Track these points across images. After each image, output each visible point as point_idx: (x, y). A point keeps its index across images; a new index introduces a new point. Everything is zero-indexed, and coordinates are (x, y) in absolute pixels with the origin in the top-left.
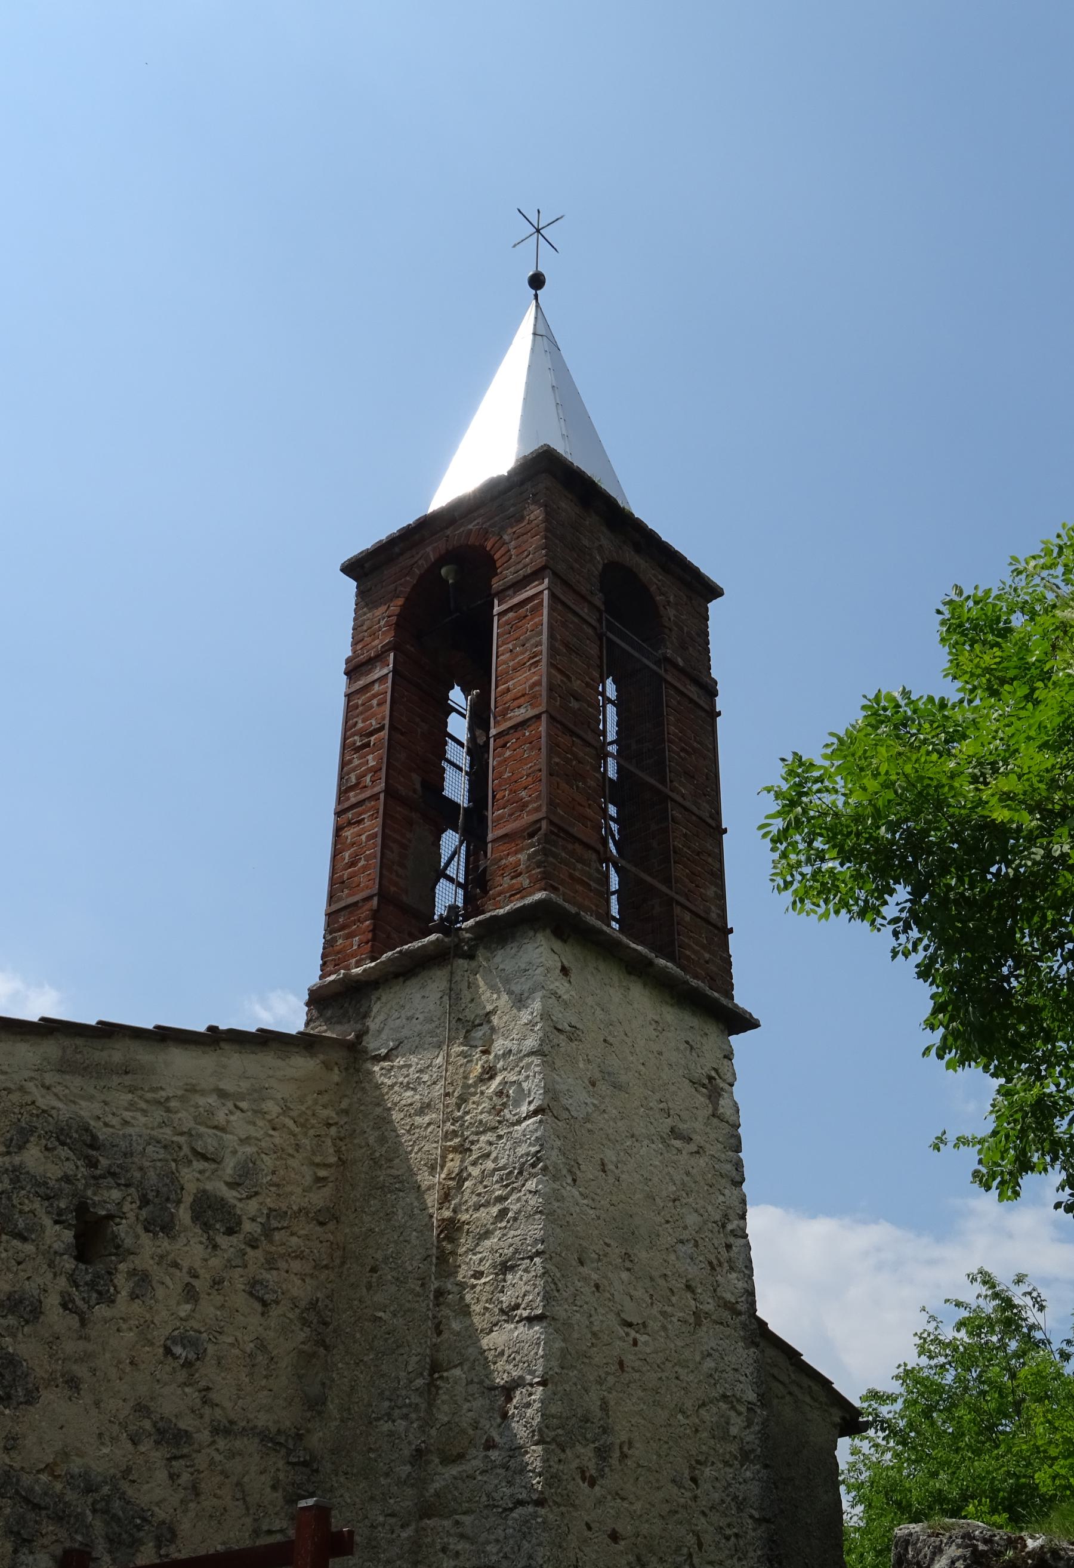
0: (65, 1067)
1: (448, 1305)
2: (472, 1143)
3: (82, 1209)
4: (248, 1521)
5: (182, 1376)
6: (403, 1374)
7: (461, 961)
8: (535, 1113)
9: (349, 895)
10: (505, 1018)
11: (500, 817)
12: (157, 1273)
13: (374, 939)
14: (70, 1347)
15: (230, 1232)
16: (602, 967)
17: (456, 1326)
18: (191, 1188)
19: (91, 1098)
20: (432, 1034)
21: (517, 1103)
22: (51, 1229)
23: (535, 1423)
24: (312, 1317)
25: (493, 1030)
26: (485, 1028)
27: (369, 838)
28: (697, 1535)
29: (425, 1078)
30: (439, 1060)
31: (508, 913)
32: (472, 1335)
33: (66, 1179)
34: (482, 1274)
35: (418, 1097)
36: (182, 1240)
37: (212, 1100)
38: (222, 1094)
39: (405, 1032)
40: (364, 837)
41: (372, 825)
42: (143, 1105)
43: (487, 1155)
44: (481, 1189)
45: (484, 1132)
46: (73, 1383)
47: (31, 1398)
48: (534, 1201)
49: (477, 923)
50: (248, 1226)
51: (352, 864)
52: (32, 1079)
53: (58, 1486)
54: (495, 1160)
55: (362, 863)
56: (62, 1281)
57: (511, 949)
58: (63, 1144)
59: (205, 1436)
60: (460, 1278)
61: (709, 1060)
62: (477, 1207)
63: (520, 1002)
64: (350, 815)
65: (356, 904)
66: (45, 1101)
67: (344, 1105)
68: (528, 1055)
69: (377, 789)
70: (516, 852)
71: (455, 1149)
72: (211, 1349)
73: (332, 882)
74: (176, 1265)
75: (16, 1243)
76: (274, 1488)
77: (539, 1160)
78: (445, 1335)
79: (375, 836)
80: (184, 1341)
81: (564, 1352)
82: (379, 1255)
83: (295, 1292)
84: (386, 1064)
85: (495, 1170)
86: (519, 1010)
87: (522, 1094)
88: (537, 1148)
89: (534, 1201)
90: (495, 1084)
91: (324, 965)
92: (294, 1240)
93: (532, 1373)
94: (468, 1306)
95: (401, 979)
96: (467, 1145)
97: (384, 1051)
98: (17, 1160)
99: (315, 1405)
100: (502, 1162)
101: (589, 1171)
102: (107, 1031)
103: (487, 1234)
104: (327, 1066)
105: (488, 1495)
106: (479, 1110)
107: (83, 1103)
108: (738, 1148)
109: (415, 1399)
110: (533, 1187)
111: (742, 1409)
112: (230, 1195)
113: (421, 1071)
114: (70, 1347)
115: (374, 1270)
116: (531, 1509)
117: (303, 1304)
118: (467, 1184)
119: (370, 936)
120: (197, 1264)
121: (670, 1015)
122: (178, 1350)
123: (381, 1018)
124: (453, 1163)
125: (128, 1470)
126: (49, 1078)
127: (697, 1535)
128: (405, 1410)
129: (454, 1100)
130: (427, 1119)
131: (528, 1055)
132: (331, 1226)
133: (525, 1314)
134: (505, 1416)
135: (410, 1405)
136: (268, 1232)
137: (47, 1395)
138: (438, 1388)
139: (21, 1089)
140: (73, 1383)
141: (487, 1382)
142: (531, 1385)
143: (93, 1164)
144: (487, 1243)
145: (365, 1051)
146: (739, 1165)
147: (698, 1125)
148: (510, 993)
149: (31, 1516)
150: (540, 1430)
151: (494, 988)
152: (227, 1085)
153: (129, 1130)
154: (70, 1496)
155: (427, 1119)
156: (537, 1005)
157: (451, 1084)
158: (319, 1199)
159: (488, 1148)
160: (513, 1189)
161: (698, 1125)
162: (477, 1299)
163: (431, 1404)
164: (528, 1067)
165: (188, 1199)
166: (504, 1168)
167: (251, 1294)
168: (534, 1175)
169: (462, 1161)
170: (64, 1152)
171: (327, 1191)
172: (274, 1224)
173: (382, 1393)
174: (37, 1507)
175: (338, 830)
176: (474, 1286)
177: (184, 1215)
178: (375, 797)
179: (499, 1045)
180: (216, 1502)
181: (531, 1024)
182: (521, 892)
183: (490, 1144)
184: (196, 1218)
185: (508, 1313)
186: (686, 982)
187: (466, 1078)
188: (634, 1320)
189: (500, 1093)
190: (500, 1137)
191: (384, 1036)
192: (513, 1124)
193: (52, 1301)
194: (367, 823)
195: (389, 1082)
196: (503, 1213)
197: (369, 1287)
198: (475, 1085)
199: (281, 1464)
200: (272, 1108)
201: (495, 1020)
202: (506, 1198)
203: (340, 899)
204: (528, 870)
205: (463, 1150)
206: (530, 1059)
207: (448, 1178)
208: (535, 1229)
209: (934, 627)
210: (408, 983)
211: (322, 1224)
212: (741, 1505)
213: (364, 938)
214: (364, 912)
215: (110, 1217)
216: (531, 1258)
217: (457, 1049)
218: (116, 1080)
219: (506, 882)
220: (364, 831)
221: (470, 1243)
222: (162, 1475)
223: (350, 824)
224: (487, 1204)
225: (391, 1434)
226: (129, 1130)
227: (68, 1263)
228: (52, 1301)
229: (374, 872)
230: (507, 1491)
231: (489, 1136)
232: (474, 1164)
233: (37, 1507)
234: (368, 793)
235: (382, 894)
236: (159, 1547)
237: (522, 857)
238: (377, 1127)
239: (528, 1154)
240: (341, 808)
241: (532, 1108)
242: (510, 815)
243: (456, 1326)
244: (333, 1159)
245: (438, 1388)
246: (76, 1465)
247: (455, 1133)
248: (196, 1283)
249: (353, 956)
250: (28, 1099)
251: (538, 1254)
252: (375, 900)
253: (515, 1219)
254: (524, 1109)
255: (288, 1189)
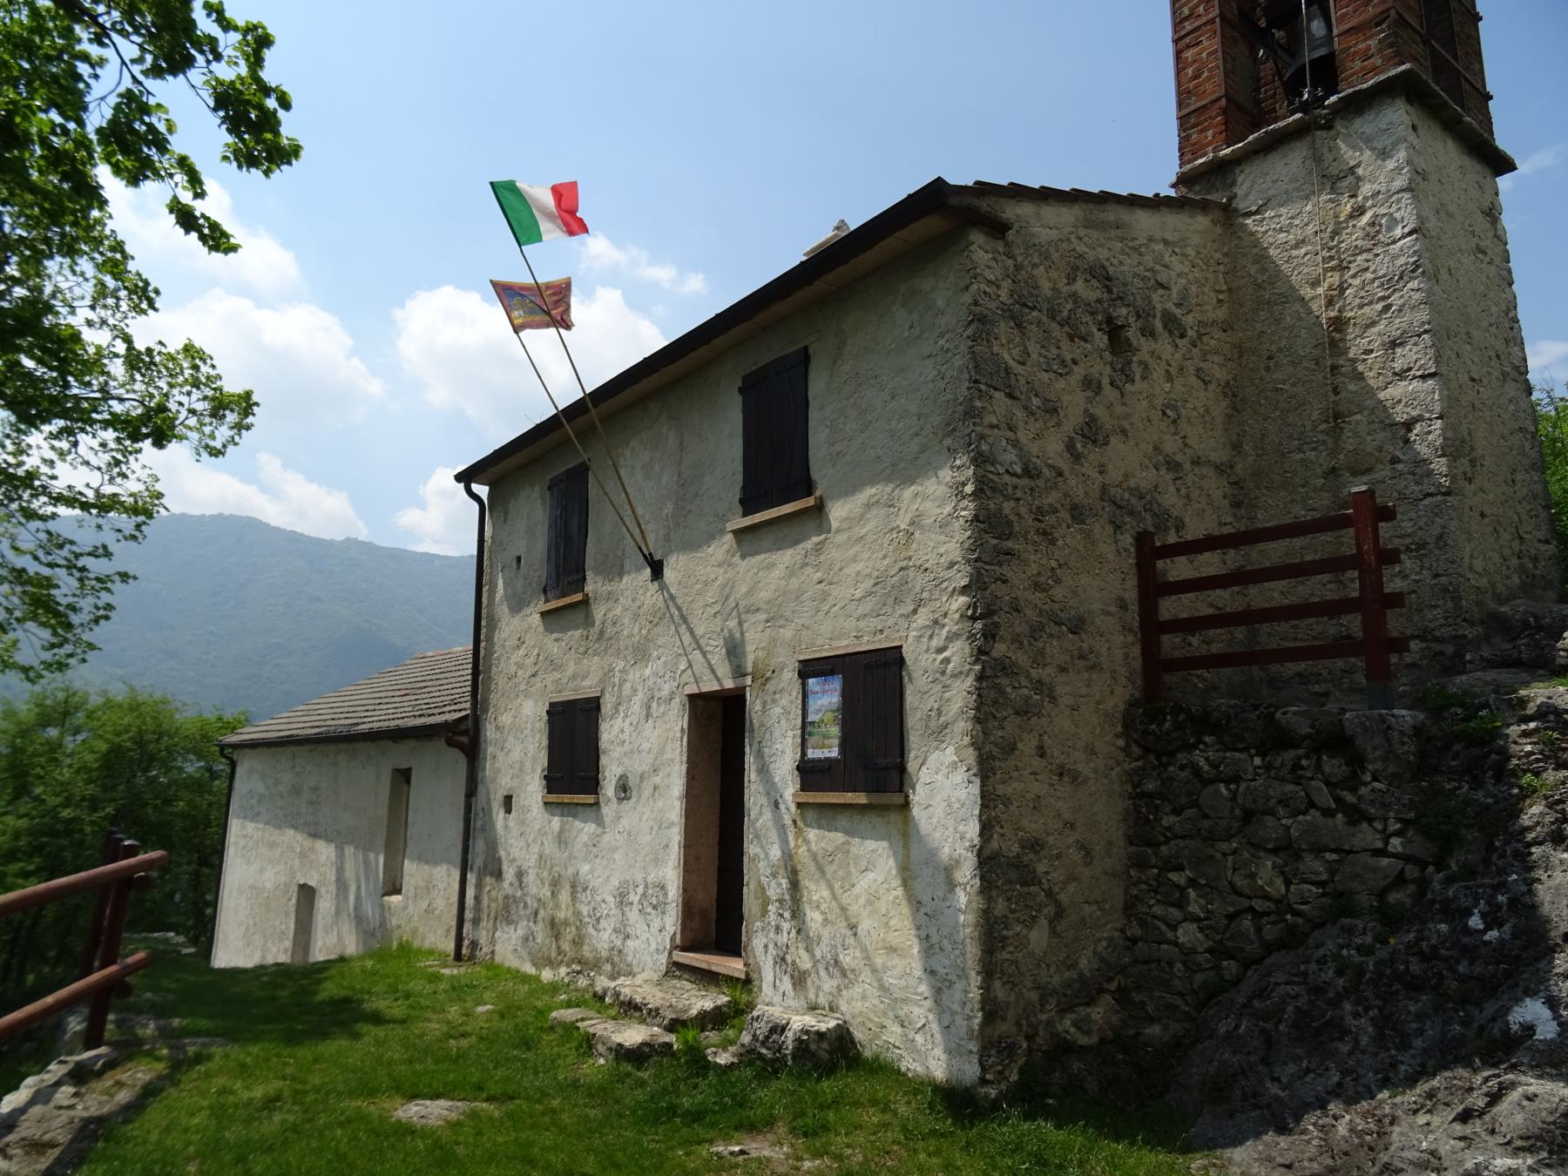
0: (1089, 224)
1: (1343, 375)
2: (1350, 262)
3: (1110, 320)
4: (1215, 516)
5: (1172, 428)
6: (1307, 423)
7: (1318, 133)
8: (1410, 234)
9: (1196, 101)
10: (1370, 169)
11: (1344, 15)
12: (1152, 362)
13: (1226, 130)
14: (1119, 410)
15: (1182, 336)
16: (1432, 125)
17: (1352, 387)
18: (1159, 306)
19: (1102, 246)
20: (1298, 190)
21: (1390, 229)
22: (1098, 334)
23: (1438, 443)
24: (1227, 391)
25: (1359, 179)
26: (1350, 179)
27: (1209, 54)
28: (1518, 515)
29: (1297, 222)
30: (1309, 208)
31: (1372, 86)
32: (1370, 392)
33: (1099, 301)
34: (1372, 351)
35: (1292, 237)
36: (1160, 342)
37: (1161, 246)
38: (1166, 242)
39: (1272, 192)
40: (1204, 55)
41: (1210, 44)
42: (1127, 250)
43: (1366, 269)
44: (1362, 293)
45: (1360, 253)
46: (1124, 432)
47: (1106, 443)
48: (1417, 296)
49: (1340, 99)
50: (1190, 332)
51: (1196, 77)
52: (1072, 233)
53: (1127, 495)
54: (1375, 271)
55: (1206, 74)
56: (1108, 368)
57: (1369, 116)
58: (1094, 277)
59: (1188, 466)
60: (1351, 355)
61: (1488, 198)
62: (1361, 306)
63: (1384, 154)
64: (1187, 40)
65: (1204, 106)
66: (1081, 248)
67: (1225, 250)
68: (1398, 192)
69: (1211, 16)
70: (1365, 40)
71: (1333, 269)
72: (1183, 411)
73: (1179, 93)
74: (1160, 358)
75: (1082, 343)
76: (1224, 497)
77: (1418, 267)
78: (1343, 395)
79: (1216, 51)
80: (1169, 406)
81: (1449, 397)
82: (1273, 347)
83: (1218, 376)
84: (1258, 217)
85: (1375, 279)
86: (1384, 160)
87: (1394, 222)
88: (1415, 258)
89: (1417, 296)
90: (1366, 219)
91: (1182, 156)
92: (1213, 342)
93: (1431, 412)
94: (1362, 373)
95: (1261, 155)
96: (1345, 264)
97: (1254, 208)
98: (1073, 288)
99: (1236, 447)
100: (1381, 273)
101: (1444, 275)
102: (1105, 198)
103: (1373, 324)
104: (1214, 222)
105: (1399, 493)
106: (1353, 237)
107: (1100, 250)
108: (1508, 262)
109: (1321, 437)
110: (1416, 286)
111: (1529, 436)
112: (1177, 312)
113: (1292, 218)
114: (1119, 410)
115: (1270, 358)
116: (1440, 498)
117: (1223, 383)
118: (1348, 292)
119: (1223, 127)
120: (1169, 357)
121: (1469, 163)
122: (1169, 412)
123: (1248, 184)
124: (1334, 278)
125: (1156, 487)
126: (1082, 232)
127: (1518, 515)
128: (1313, 445)
129: (1327, 234)
130: (1303, 251)
131: (1398, 192)
132: (1230, 332)
133: (1420, 373)
134: (1407, 441)
135: (1318, 441)
136: (1200, 335)
137: (1114, 440)
138: (1342, 429)
139: (1068, 240)
140: (1124, 432)
141: (1388, 421)
142: (1431, 420)
143: (1110, 291)
144: (1375, 330)
145: (1236, 210)
146: (1509, 271)
147: (1488, 243)
148: (1372, 149)
149: (1118, 512)
150: (1442, 448)
151: (1355, 148)
152: (1168, 236)
153: (1123, 268)
154: (1134, 501)
155: (1303, 251)
156: (1402, 155)
157: (1323, 223)
158: (1221, 314)
159: (1366, 265)
160: (1395, 290)
161: (1488, 243)
162: (1371, 370)
163: (1337, 440)
164: (1399, 200)
165: (1159, 315)
166: (1384, 276)
167: (1198, 377)
168: (1415, 278)
169: (1341, 276)
170: (1095, 283)
171: (1225, 309)
172: (1203, 331)
173: (1291, 435)
174: (1120, 507)
175: (1178, 55)
176: (1365, 360)
177: (1158, 324)
178: (1212, 21)
179: (1366, 189)
180: (1198, 506)
181: (1398, 169)
182: (1375, 70)
183: (1368, 261)
184: (1165, 327)
185: (1401, 375)
186: (1481, 135)
187: (1337, 217)
188: (1476, 377)
189: (1373, 224)
190: (1377, 255)
191: (1252, 197)
192: (1388, 245)
193: (1106, 381)
194: (1205, 44)
195: (1263, 229)
196: (1387, 308)
197: (1268, 369)
198: (1346, 221)
199: (1225, 483)
200: (1190, 251)
201: (1360, 171)
202: (1389, 297)
203: (1188, 105)
204: (1380, 51)
205: (1341, 268)
206: (1400, 195)
207: (1330, 288)
208: (1423, 315)
209: (247, 388)
210: (1269, 156)
211: (1225, 331)
212: (1535, 497)
213: (1218, 130)
214: (1215, 110)
215: (1123, 327)
216: (1419, 336)
217: (1324, 197)
218: (1113, 233)
219: (1358, 64)
220: (1204, 50)
221: (1358, 331)
222: (1172, 489)
223: (1188, 47)
224: (1371, 303)
225: (1303, 460)
226: (1123, 268)
227: (1108, 356)
228: (1106, 381)
229: (1219, 78)
230: (1418, 488)
231: (1365, 256)
232: (1354, 276)
233: (1120, 507)
234: (1204, 20)
235: (1227, 96)
236: (1177, 532)
237: (1373, 42)
238: (1255, 262)
239: (1407, 264)
240: (1176, 37)
241: (1406, 230)
242: (1355, 11)
243: (1352, 387)
244: (1225, 288)
245: (1342, 429)
246: (1132, 483)
247: (1332, 258)
248: (1171, 369)
249: (1209, 144)
250: (1071, 247)
251: (1426, 332)
252: (1223, 101)
253: (1400, 311)
254: (1398, 232)
255: (1206, 307)
